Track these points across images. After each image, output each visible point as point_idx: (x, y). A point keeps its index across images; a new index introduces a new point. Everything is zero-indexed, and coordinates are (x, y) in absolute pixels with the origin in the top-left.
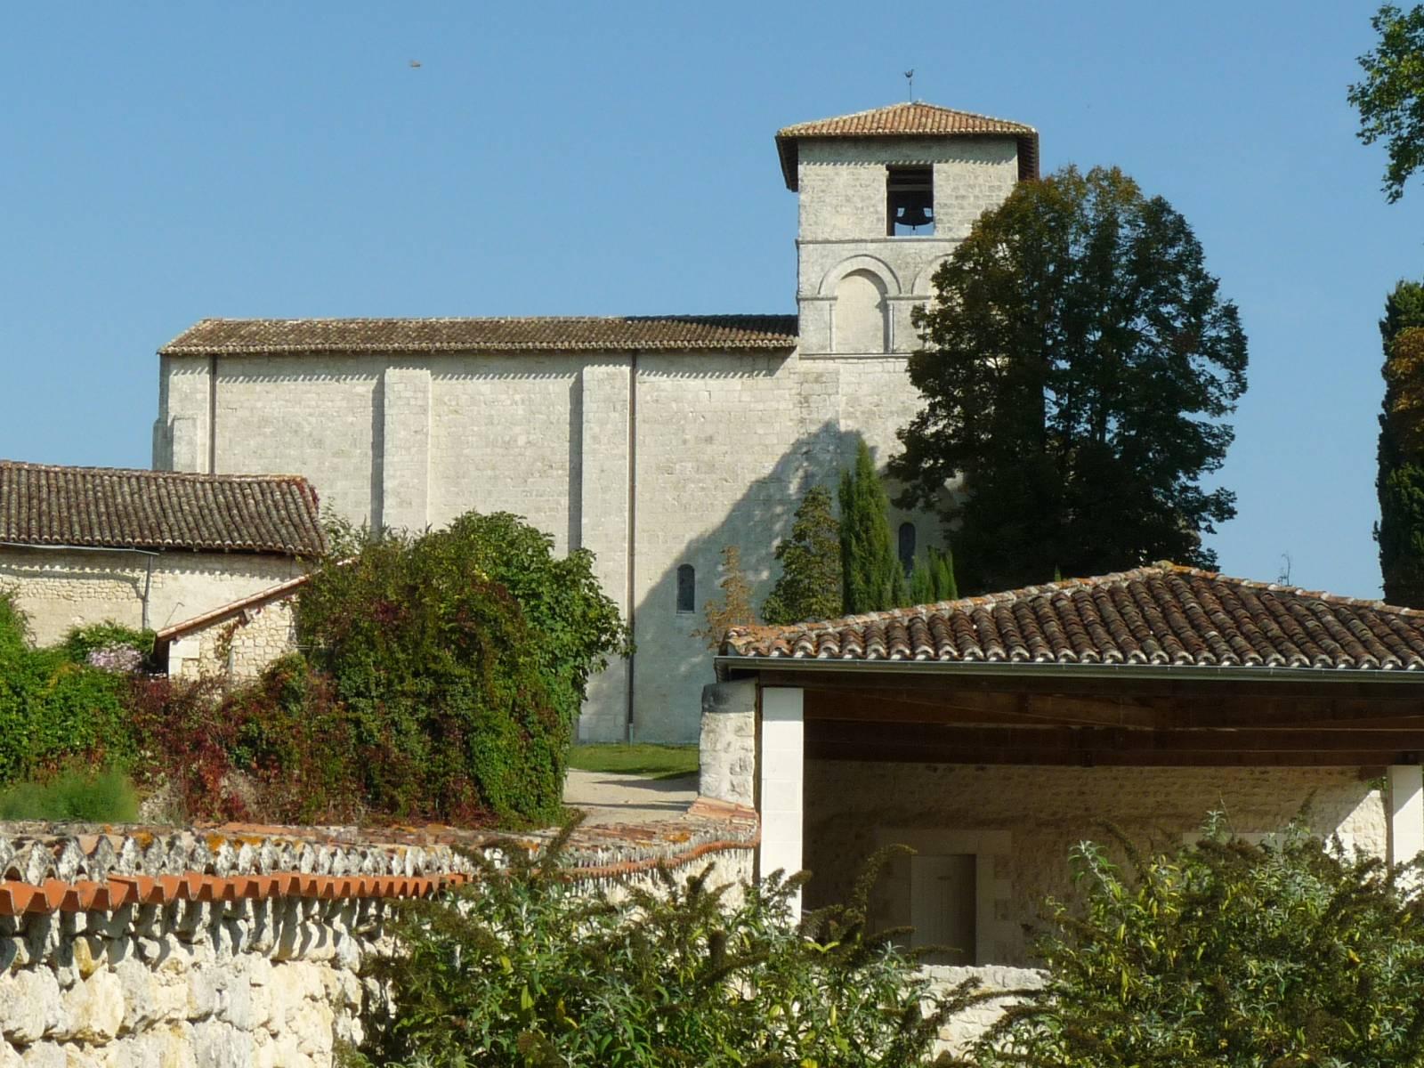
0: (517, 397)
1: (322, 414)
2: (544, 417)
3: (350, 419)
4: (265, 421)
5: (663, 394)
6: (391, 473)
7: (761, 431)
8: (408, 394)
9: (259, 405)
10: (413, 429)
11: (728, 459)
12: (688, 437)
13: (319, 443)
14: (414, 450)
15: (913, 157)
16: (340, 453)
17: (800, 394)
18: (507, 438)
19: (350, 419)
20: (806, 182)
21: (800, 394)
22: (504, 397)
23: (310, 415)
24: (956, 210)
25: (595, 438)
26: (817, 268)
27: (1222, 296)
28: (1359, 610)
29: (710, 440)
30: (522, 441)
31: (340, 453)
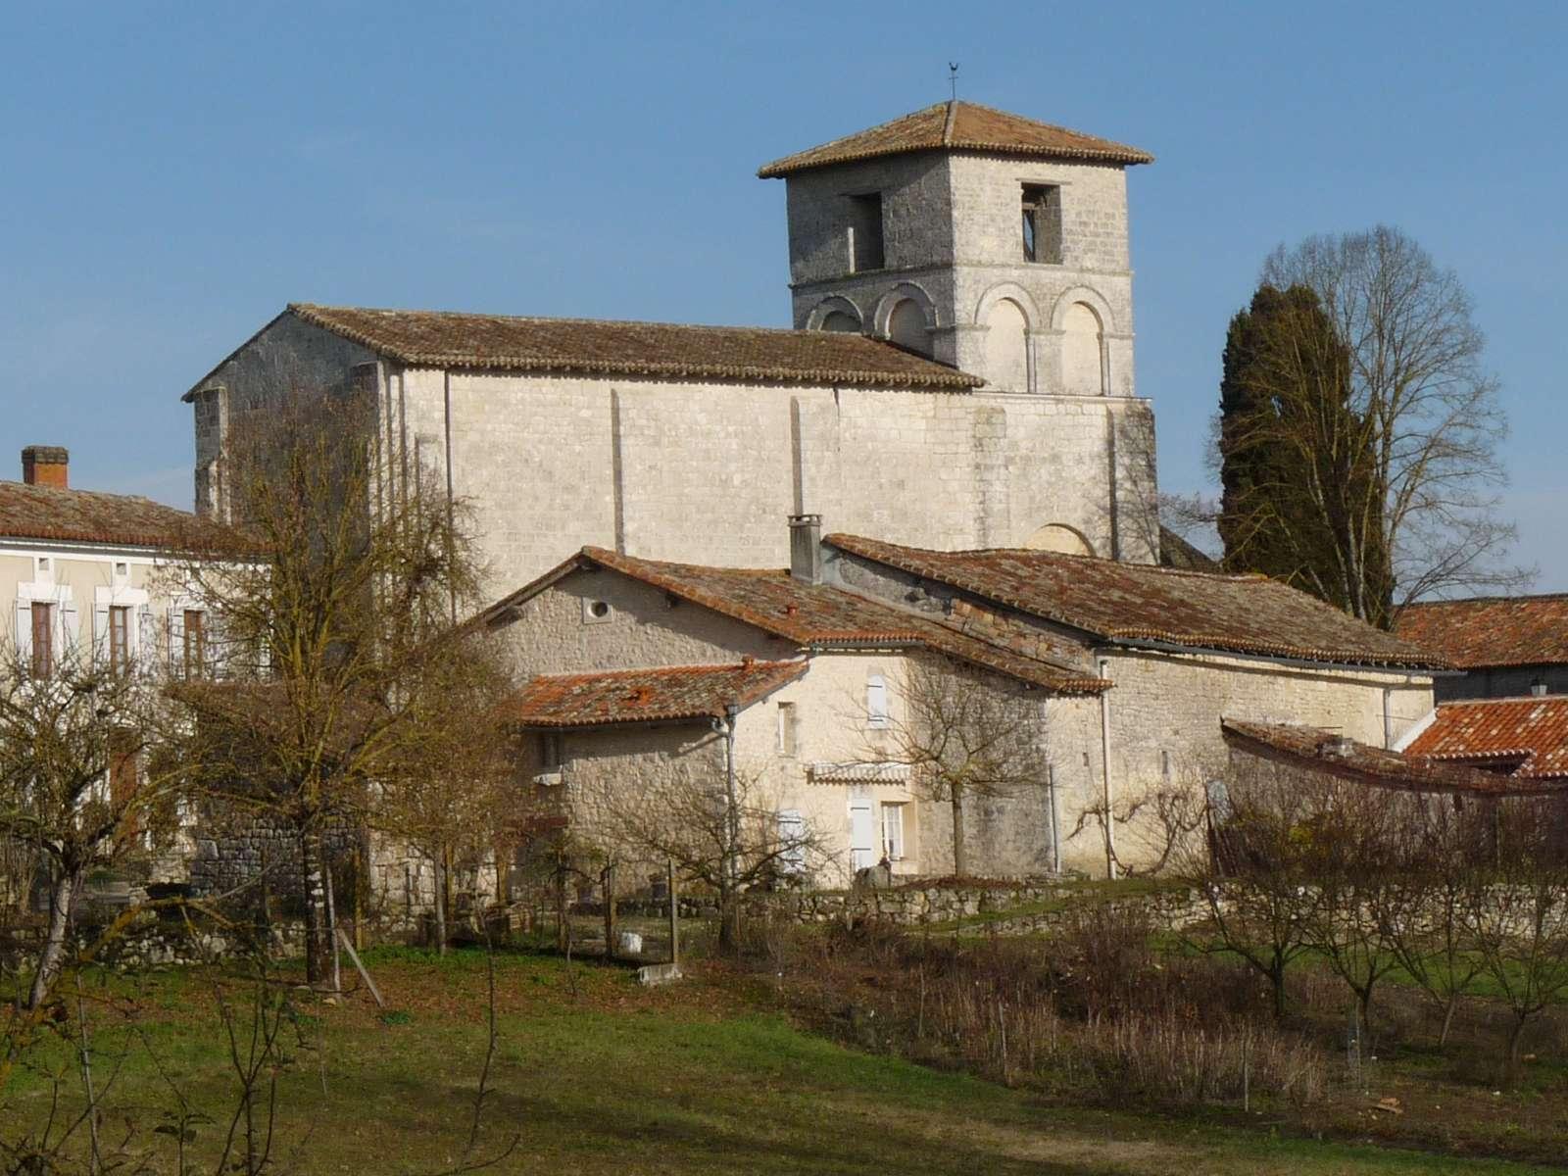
0: (731, 429)
1: (551, 441)
2: (754, 453)
3: (578, 448)
4: (495, 447)
5: (860, 431)
6: (631, 514)
7: (944, 477)
8: (643, 422)
9: (489, 427)
10: (648, 463)
11: (918, 507)
12: (883, 481)
13: (549, 475)
14: (650, 488)
15: (865, 182)
16: (570, 489)
17: (974, 437)
18: (724, 477)
19: (578, 448)
20: (957, 197)
21: (974, 437)
22: (718, 428)
23: (540, 441)
24: (1080, 237)
25: (812, 479)
26: (972, 295)
27: (1486, 362)
28: (196, 408)
29: (901, 484)
30: (736, 481)
31: (570, 489)
